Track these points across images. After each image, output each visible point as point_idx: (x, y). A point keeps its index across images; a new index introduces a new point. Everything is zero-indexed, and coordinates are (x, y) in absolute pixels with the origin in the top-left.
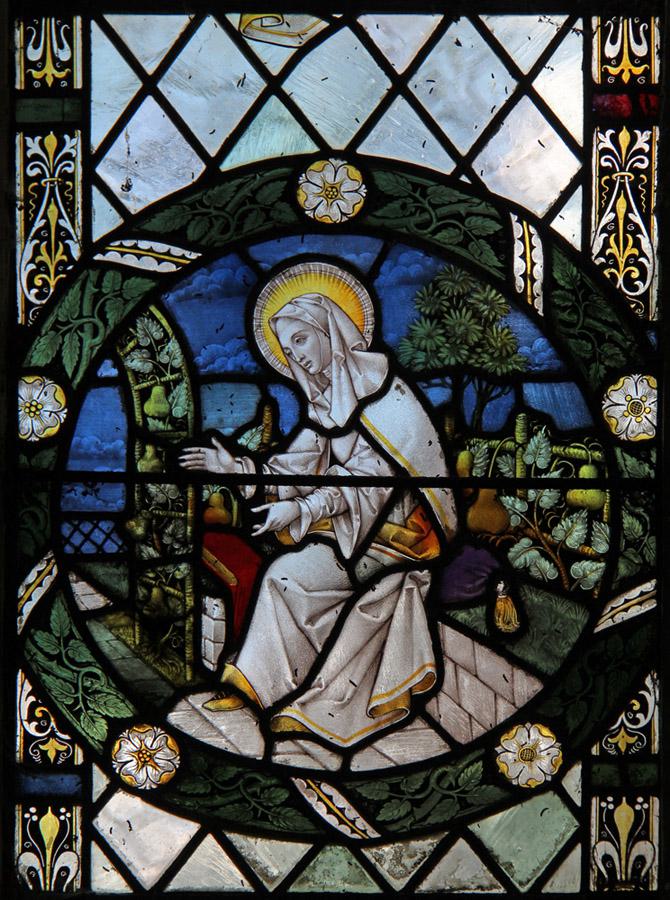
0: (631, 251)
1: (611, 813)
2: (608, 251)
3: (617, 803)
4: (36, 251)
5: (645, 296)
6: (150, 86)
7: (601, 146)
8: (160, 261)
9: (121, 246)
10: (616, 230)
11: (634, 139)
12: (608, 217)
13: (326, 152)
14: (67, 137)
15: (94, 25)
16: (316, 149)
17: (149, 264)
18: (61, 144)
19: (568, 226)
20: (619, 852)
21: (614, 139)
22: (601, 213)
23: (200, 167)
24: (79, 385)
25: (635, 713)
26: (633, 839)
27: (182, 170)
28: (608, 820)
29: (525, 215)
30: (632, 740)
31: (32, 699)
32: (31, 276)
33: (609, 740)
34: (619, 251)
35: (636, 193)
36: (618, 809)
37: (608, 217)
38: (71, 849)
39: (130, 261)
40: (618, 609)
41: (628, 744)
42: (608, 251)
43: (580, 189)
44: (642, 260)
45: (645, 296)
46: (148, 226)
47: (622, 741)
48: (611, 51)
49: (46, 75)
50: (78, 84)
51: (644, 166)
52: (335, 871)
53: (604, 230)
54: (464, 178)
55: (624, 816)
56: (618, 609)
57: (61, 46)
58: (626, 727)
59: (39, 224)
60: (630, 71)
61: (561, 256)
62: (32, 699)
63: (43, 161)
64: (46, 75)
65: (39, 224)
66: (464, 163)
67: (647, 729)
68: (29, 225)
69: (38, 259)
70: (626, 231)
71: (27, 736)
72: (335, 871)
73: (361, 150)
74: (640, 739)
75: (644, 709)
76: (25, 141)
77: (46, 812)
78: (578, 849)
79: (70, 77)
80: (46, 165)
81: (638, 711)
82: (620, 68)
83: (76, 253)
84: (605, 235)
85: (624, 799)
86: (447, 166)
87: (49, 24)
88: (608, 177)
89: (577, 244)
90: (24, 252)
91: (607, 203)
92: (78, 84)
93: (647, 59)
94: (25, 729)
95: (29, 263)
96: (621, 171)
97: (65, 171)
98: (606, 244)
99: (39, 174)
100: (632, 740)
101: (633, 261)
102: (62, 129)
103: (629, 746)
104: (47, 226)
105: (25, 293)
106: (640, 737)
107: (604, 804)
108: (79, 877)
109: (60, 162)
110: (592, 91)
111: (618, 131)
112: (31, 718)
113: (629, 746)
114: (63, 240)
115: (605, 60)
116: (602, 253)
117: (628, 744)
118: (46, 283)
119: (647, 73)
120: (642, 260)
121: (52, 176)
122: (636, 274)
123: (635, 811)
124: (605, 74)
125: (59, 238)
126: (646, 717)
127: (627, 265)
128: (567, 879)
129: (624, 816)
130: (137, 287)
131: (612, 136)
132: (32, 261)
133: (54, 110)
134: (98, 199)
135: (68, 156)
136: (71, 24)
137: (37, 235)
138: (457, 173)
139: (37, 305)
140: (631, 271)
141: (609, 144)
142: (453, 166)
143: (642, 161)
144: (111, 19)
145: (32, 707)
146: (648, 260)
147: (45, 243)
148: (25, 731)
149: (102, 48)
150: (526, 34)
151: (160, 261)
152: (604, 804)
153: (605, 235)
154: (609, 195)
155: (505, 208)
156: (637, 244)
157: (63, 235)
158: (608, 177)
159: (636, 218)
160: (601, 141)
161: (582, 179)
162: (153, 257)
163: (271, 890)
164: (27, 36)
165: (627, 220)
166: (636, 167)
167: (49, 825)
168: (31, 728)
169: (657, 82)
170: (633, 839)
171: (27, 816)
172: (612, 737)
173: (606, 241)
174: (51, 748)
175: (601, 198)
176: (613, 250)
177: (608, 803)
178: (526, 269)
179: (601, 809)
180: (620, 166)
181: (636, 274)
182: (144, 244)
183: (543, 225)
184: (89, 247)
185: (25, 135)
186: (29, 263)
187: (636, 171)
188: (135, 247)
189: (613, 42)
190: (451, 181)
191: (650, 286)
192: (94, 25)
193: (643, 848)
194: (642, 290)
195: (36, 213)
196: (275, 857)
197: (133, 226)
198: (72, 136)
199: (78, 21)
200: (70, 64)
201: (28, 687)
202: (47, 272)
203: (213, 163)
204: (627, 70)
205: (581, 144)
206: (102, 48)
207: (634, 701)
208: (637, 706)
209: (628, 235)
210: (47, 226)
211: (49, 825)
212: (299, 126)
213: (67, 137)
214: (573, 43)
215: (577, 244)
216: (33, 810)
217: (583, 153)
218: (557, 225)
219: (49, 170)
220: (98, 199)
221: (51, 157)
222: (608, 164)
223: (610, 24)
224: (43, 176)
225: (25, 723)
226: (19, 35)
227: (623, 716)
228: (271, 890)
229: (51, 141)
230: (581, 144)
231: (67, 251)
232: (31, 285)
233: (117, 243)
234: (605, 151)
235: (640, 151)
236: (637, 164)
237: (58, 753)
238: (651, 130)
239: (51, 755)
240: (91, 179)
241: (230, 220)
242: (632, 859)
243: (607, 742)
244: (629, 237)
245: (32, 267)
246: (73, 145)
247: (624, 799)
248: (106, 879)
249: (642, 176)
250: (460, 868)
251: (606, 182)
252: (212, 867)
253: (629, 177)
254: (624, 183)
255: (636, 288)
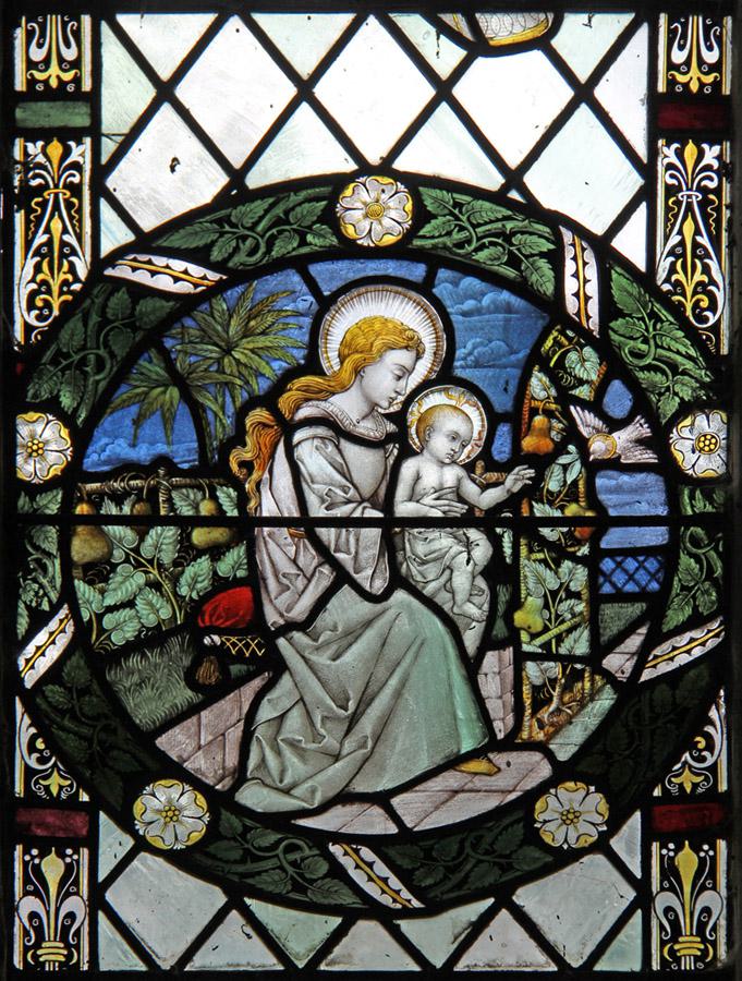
0: (699, 277)
1: (671, 859)
2: (674, 278)
3: (679, 848)
4: (38, 269)
5: (716, 328)
6: (165, 92)
7: (666, 161)
8: (176, 279)
9: (135, 260)
10: (684, 255)
11: (701, 154)
12: (674, 239)
13: (365, 168)
14: (72, 144)
15: (105, 28)
16: (355, 167)
17: (164, 283)
18: (67, 152)
19: (631, 244)
20: (683, 905)
21: (680, 154)
22: (667, 238)
23: (223, 179)
24: (85, 421)
25: (701, 751)
26: (699, 889)
27: (208, 184)
28: (670, 871)
29: (580, 231)
30: (697, 780)
31: (33, 730)
32: (32, 296)
33: (673, 779)
34: (686, 276)
35: (706, 217)
36: (680, 854)
37: (674, 239)
38: (77, 894)
39: (142, 277)
40: (681, 650)
41: (693, 784)
42: (674, 278)
43: (643, 206)
44: (712, 288)
45: (716, 328)
46: (164, 243)
47: (687, 780)
48: (679, 57)
49: (50, 76)
50: (87, 85)
51: (712, 185)
52: (368, 947)
53: (672, 253)
54: (514, 195)
55: (687, 861)
56: (681, 650)
57: (68, 45)
58: (690, 767)
59: (41, 239)
60: (699, 79)
61: (624, 282)
62: (33, 730)
63: (45, 168)
64: (50, 76)
65: (41, 239)
66: (514, 177)
67: (713, 769)
68: (28, 243)
69: (39, 277)
70: (694, 255)
71: (27, 767)
72: (368, 947)
73: (400, 164)
74: (707, 779)
75: (710, 747)
76: (25, 147)
77: (50, 852)
78: (638, 874)
79: (77, 80)
80: (49, 173)
81: (704, 750)
82: (688, 76)
83: (82, 272)
84: (671, 259)
85: (687, 842)
86: (493, 180)
87: (54, 23)
88: (674, 198)
89: (641, 265)
90: (24, 270)
91: (673, 225)
92: (87, 85)
93: (717, 67)
94: (26, 764)
95: (29, 282)
96: (688, 190)
97: (71, 183)
98: (672, 270)
99: (41, 184)
100: (697, 780)
101: (701, 287)
102: (68, 135)
103: (695, 786)
104: (49, 243)
105: (22, 315)
106: (706, 776)
107: (664, 852)
108: (86, 922)
109: (67, 168)
110: (655, 102)
111: (684, 145)
112: (32, 748)
113: (695, 786)
114: (66, 256)
115: (671, 66)
116: (667, 280)
117: (693, 784)
118: (48, 305)
119: (717, 85)
120: (712, 288)
121: (56, 186)
122: (705, 304)
123: (699, 858)
124: (672, 82)
125: (62, 256)
126: (712, 754)
127: (695, 293)
128: (625, 957)
129: (687, 861)
130: (78, 671)
131: (676, 150)
132: (33, 280)
133: (56, 115)
134: (106, 212)
135: (77, 166)
136: (79, 22)
137: (37, 253)
138: (505, 188)
139: (38, 328)
140: (698, 301)
141: (674, 160)
142: (501, 180)
143: (711, 179)
144: (127, 21)
145: (33, 739)
146: (718, 288)
147: (46, 260)
148: (26, 765)
149: (112, 50)
150: (583, 38)
151: (176, 279)
152: (664, 852)
153: (671, 259)
154: (676, 216)
155: (555, 220)
156: (706, 270)
157: (67, 251)
158: (674, 198)
159: (704, 240)
160: (666, 156)
161: (646, 194)
162: (173, 276)
163: (300, 967)
164: (30, 35)
165: (696, 245)
166: (705, 186)
167: (52, 868)
168: (33, 763)
169: (728, 93)
170: (699, 889)
171: (27, 858)
172: (676, 776)
173: (673, 265)
174: (55, 782)
175: (666, 226)
176: (680, 276)
177: (669, 850)
178: (579, 308)
179: (662, 857)
180: (687, 184)
181: (705, 304)
182: (160, 261)
183: (602, 247)
184: (99, 264)
185: (26, 141)
186: (29, 282)
187: (704, 190)
188: (150, 262)
189: (681, 48)
190: (498, 197)
191: (722, 315)
192: (105, 28)
193: (707, 898)
194: (712, 321)
195: (37, 227)
196: (302, 932)
197: (146, 243)
198: (79, 143)
199: (86, 20)
200: (76, 64)
201: (27, 720)
202: (49, 292)
203: (237, 176)
204: (693, 79)
205: (645, 161)
206: (112, 50)
207: (698, 739)
208: (702, 745)
209: (697, 261)
210: (49, 243)
211: (52, 868)
212: (291, 481)
213: (72, 144)
214: (642, 35)
215: (641, 265)
216: (35, 852)
217: (647, 170)
218: (620, 243)
219: (53, 179)
220: (106, 212)
221: (55, 166)
222: (675, 182)
223: (676, 27)
224: (45, 187)
225: (26, 757)
226: (20, 34)
227: (687, 755)
228: (300, 967)
229: (55, 149)
230: (645, 161)
231: (72, 269)
232: (31, 306)
233: (132, 257)
234: (670, 166)
235: (708, 168)
236: (704, 183)
237: (61, 787)
238: (721, 144)
239: (54, 791)
240: (100, 190)
241: (260, 239)
242: (698, 908)
243: (670, 782)
244: (697, 261)
245: (34, 286)
246: (81, 152)
247: (687, 842)
248: (115, 956)
249: (712, 197)
250: (504, 946)
251: (674, 203)
252: (236, 949)
253: (697, 197)
254: (692, 202)
255: (706, 320)
